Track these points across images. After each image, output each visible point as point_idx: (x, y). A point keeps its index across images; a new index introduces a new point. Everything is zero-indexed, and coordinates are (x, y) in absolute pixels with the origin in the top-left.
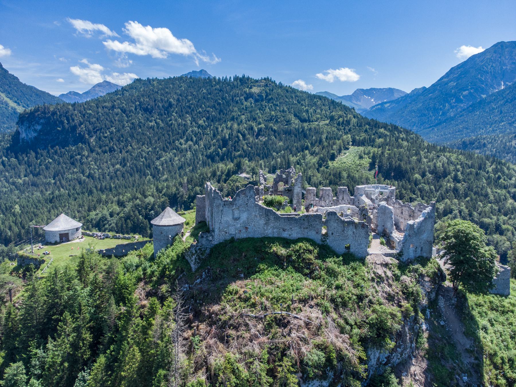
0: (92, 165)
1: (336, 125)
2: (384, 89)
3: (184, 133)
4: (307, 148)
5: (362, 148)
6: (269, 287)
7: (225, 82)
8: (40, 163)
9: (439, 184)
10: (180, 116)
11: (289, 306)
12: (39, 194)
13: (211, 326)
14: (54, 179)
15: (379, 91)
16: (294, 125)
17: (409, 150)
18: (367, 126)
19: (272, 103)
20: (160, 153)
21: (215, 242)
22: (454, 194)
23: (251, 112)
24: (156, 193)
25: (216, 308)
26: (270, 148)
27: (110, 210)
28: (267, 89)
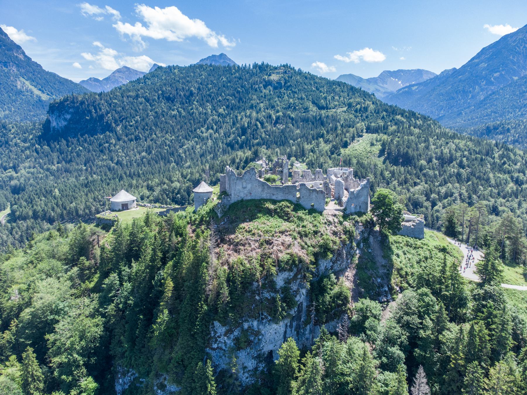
0: (120, 152)
1: (353, 112)
2: (412, 70)
3: (205, 121)
4: (322, 136)
5: (375, 136)
6: (263, 226)
7: (244, 70)
8: (71, 150)
9: (443, 169)
10: (201, 105)
11: (273, 235)
12: (74, 180)
13: (230, 245)
14: (85, 166)
15: (406, 73)
16: (311, 113)
17: (419, 137)
18: (385, 113)
19: (291, 90)
20: (182, 141)
21: (232, 202)
22: (457, 178)
23: (269, 100)
24: (181, 179)
25: (233, 236)
26: (287, 135)
27: (141, 194)
28: (286, 76)
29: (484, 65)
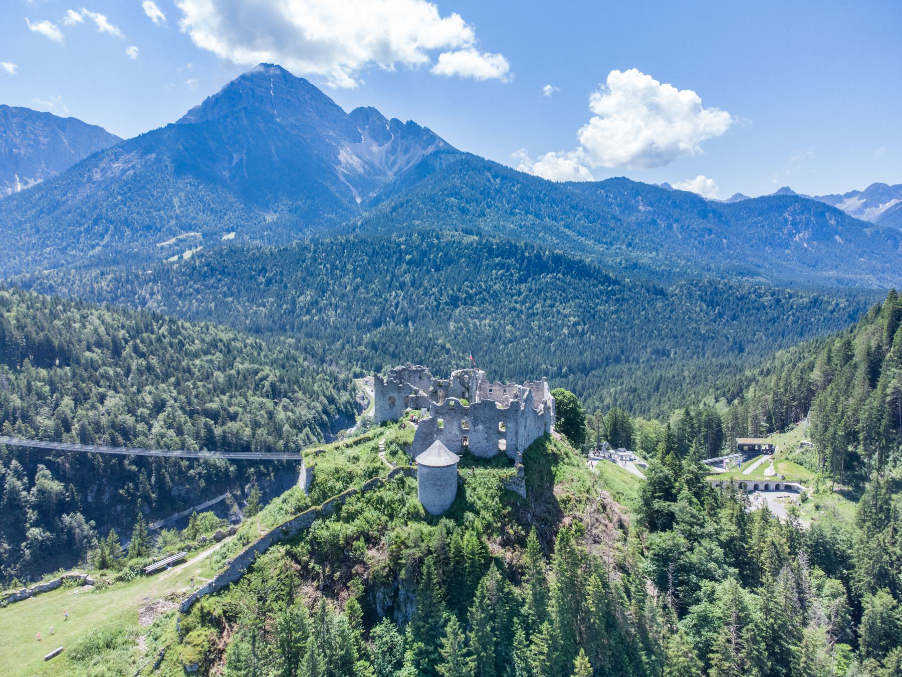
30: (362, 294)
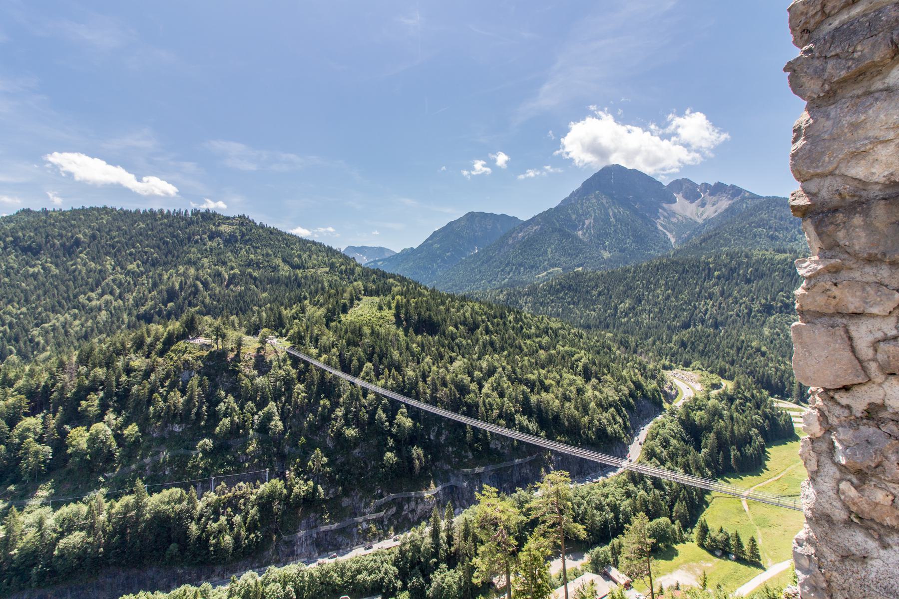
1: (338, 273)
19: (251, 245)
29: (437, 246)
30: (673, 301)
